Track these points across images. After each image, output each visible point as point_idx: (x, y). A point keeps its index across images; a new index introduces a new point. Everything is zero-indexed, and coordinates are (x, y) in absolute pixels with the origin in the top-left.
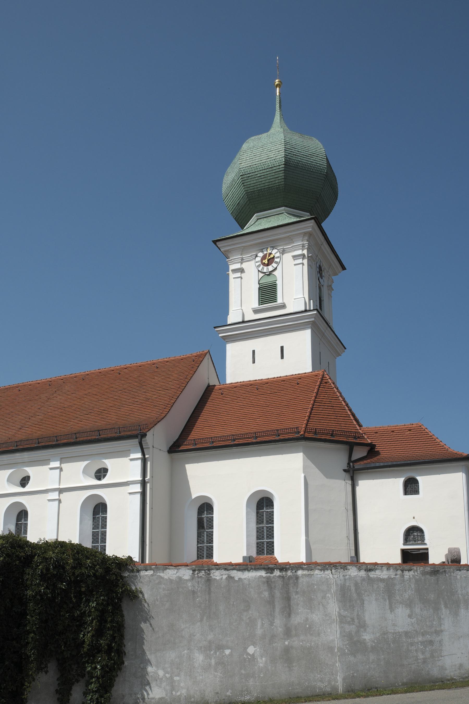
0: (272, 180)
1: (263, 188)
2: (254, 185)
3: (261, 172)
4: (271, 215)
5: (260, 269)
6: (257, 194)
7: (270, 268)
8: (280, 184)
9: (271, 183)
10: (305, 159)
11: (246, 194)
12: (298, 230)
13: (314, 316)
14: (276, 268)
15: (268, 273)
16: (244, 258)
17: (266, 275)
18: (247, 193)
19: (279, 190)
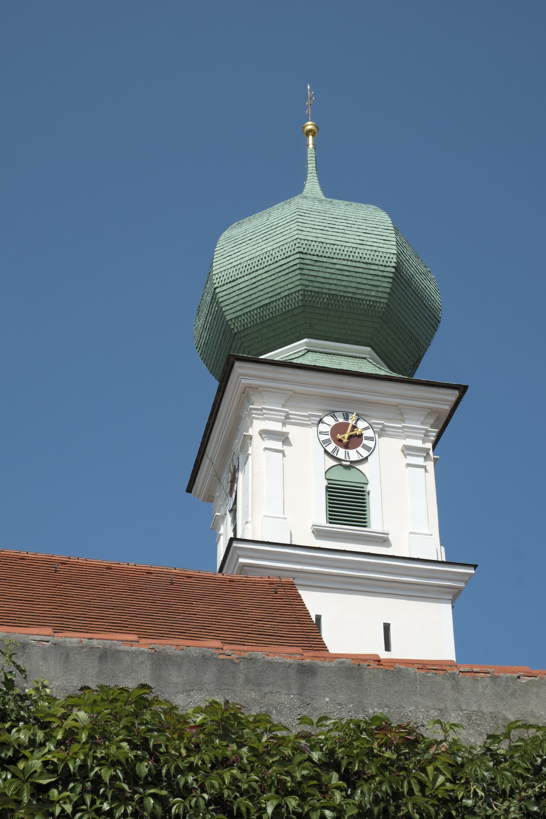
0: (363, 287)
1: (342, 294)
2: (323, 280)
3: (344, 262)
4: (340, 352)
5: (330, 449)
6: (325, 301)
7: (353, 455)
8: (378, 300)
9: (360, 291)
10: (234, 294)
11: (301, 293)
12: (434, 400)
13: (467, 578)
14: (367, 458)
15: (348, 463)
16: (291, 416)
17: (341, 465)
18: (304, 290)
19: (259, 318)
